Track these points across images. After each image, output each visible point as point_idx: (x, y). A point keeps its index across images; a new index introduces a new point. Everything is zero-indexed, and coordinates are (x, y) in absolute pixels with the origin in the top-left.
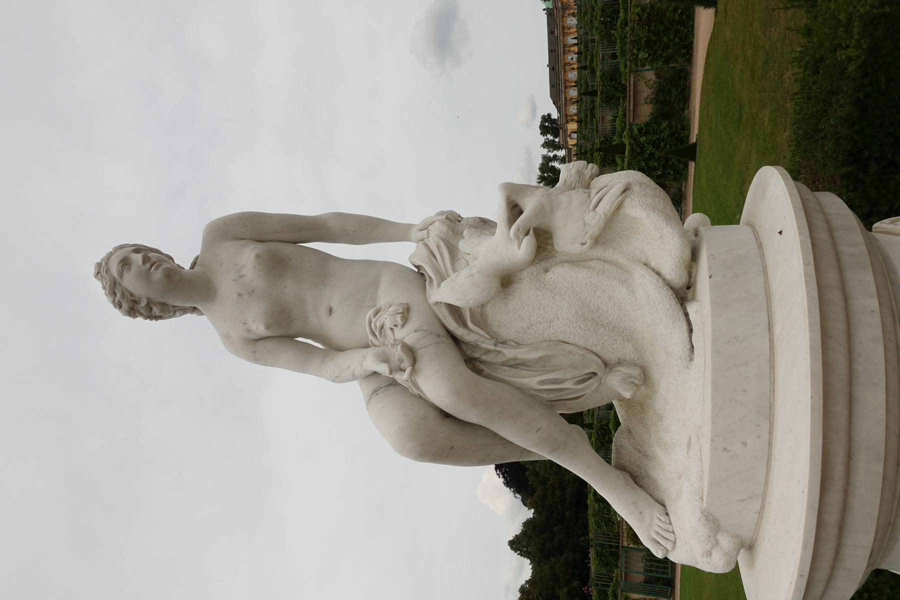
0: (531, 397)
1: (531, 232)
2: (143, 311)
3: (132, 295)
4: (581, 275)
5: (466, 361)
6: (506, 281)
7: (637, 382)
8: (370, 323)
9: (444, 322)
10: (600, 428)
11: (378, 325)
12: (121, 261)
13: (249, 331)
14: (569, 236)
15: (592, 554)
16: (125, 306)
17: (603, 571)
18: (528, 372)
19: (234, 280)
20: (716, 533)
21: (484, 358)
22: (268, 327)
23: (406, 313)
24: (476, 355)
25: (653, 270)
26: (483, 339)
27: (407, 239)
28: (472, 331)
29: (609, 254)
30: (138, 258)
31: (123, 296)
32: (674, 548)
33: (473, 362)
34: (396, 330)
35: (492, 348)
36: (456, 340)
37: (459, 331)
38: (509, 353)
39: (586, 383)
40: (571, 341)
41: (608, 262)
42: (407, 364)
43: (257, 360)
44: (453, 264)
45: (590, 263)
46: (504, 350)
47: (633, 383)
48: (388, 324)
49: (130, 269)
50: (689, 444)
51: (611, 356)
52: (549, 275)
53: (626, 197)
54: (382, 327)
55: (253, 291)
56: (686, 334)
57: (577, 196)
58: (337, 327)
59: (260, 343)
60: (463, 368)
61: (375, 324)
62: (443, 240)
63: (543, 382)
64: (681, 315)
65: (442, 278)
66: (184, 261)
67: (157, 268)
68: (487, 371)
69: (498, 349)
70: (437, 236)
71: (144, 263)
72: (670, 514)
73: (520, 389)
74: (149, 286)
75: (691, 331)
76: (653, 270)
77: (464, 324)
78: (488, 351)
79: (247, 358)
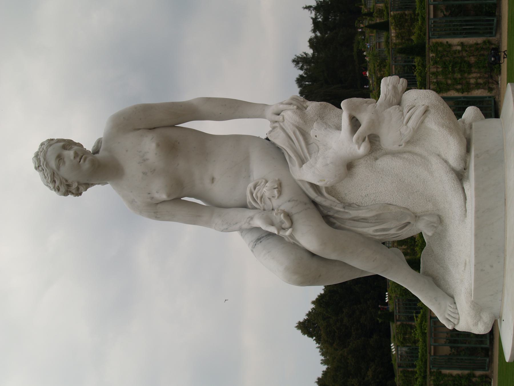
0: (369, 241)
1: (367, 139)
2: (74, 191)
3: (67, 181)
5: (323, 217)
6: (350, 166)
7: (435, 225)
8: (252, 194)
9: (307, 192)
10: (413, 250)
11: (259, 195)
13: (152, 198)
14: (389, 138)
16: (63, 189)
17: (473, 70)
18: (366, 224)
19: (139, 163)
20: (480, 313)
21: (336, 215)
22: (169, 196)
23: (280, 187)
24: (330, 214)
25: (443, 159)
27: (261, 116)
28: (328, 199)
29: (417, 149)
30: (70, 154)
31: (61, 183)
32: (458, 323)
33: (328, 218)
34: (273, 200)
35: (342, 210)
36: (315, 204)
37: (319, 199)
38: (354, 213)
39: (404, 229)
40: (394, 204)
41: (416, 154)
42: (287, 224)
43: (157, 218)
44: (308, 149)
45: (405, 156)
46: (351, 212)
47: (433, 226)
48: (267, 194)
49: (64, 163)
50: (466, 264)
51: (418, 210)
52: (378, 162)
54: (262, 197)
55: (154, 170)
56: (463, 203)
57: (393, 110)
58: (220, 190)
59: (159, 206)
60: (325, 226)
61: (256, 195)
62: (297, 127)
63: (376, 231)
64: (460, 189)
65: (302, 161)
66: (89, 146)
67: (85, 160)
68: (338, 224)
69: (346, 211)
70: (293, 125)
72: (457, 303)
73: (361, 234)
76: (443, 159)
77: (321, 194)
78: (338, 212)
79: (150, 217)
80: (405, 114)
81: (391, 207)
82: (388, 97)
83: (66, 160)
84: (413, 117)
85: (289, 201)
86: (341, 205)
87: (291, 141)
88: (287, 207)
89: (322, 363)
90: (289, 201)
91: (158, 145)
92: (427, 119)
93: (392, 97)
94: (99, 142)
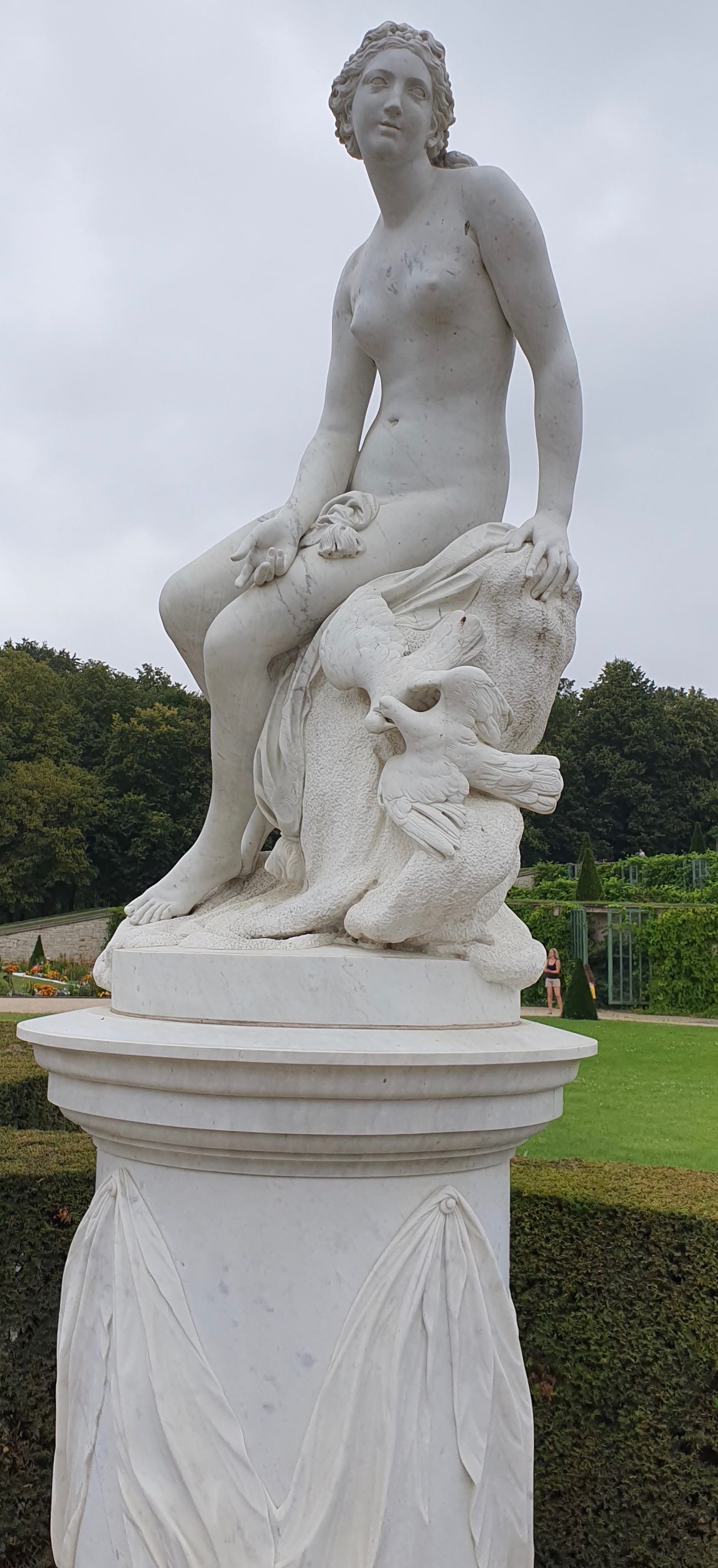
4: (360, 799)
12: (384, 72)
15: (674, 857)
26: (308, 671)
29: (386, 834)
31: (345, 94)
49: (376, 90)
53: (427, 852)
55: (396, 292)
63: (259, 753)
65: (393, 601)
67: (385, 134)
71: (387, 110)
74: (394, 112)
75: (276, 938)
80: (441, 806)
81: (298, 784)
82: (497, 771)
83: (383, 93)
84: (428, 825)
85: (308, 576)
86: (304, 683)
87: (449, 571)
88: (298, 572)
89: (148, 668)
90: (308, 576)
91: (433, 287)
92: (424, 856)
93: (499, 778)
94: (467, 162)
